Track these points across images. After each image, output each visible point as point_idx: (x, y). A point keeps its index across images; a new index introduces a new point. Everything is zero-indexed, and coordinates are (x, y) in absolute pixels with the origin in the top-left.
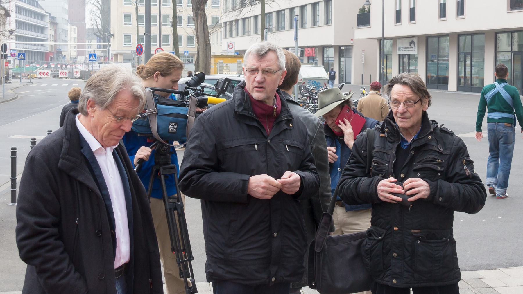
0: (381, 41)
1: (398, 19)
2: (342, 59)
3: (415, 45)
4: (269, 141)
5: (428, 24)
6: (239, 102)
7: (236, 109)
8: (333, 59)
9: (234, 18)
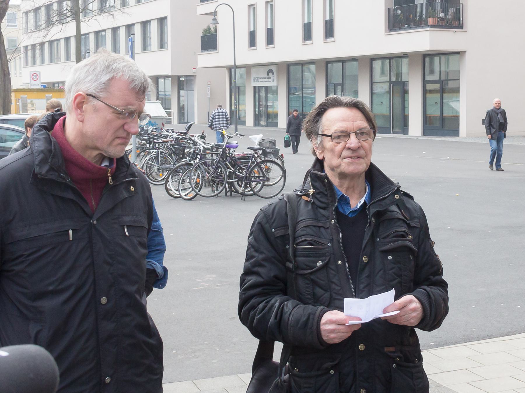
0: (230, 69)
1: (252, 42)
2: (182, 93)
3: (273, 74)
4: (95, 222)
5: (290, 48)
6: (41, 156)
7: (37, 170)
8: (170, 93)
9: (39, 40)
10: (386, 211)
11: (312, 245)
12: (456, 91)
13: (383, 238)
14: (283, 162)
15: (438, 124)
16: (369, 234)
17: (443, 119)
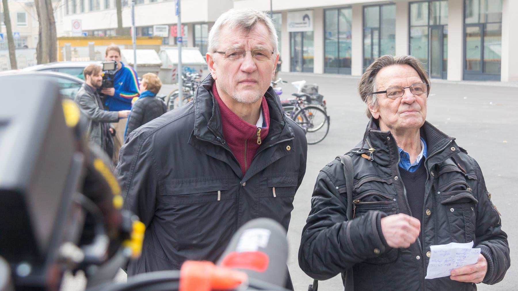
3: (309, 19)
6: (202, 118)
10: (443, 165)
11: (378, 200)
12: (498, 34)
13: (444, 191)
14: (325, 108)
15: (478, 68)
16: (430, 188)
17: (483, 63)
